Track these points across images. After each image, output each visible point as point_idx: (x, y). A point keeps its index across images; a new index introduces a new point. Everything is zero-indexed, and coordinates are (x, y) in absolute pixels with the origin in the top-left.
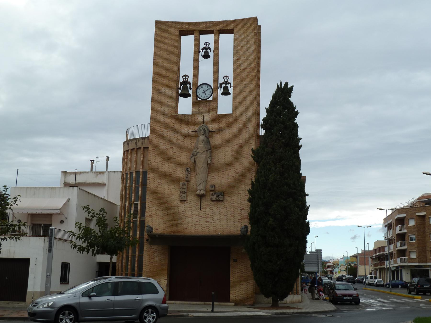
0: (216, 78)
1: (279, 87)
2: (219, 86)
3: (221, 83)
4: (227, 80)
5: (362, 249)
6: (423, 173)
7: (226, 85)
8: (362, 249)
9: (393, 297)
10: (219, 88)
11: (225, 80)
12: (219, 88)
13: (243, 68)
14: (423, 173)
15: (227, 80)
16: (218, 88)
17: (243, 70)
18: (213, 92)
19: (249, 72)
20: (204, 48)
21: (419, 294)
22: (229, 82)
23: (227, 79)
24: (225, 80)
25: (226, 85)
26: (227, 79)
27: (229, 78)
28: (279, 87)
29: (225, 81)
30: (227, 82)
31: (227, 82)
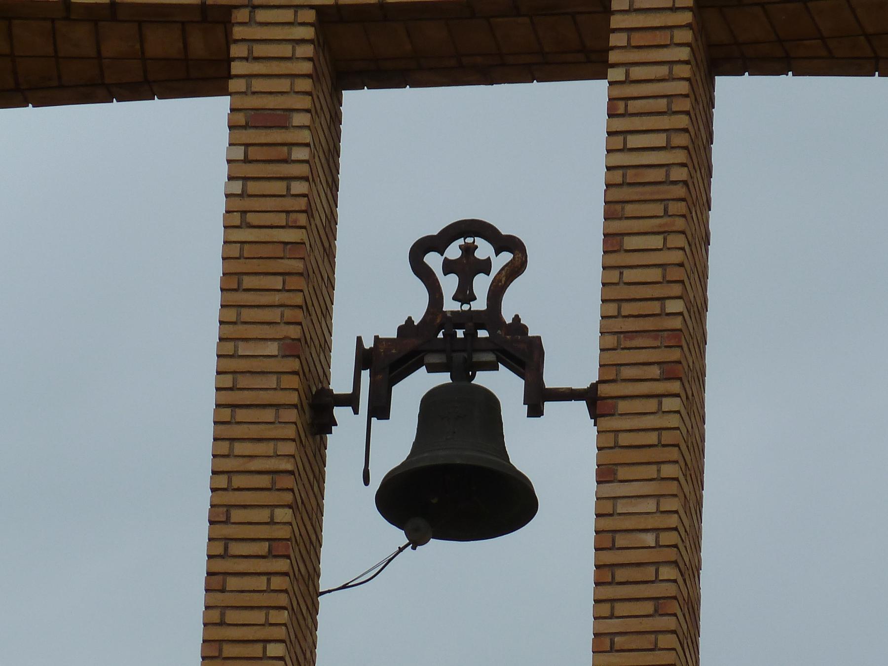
4: (480, 304)
5: (359, 340)
8: (359, 340)
12: (340, 413)
20: (407, 329)
23: (482, 284)
24: (450, 305)
26: (482, 284)
29: (459, 319)
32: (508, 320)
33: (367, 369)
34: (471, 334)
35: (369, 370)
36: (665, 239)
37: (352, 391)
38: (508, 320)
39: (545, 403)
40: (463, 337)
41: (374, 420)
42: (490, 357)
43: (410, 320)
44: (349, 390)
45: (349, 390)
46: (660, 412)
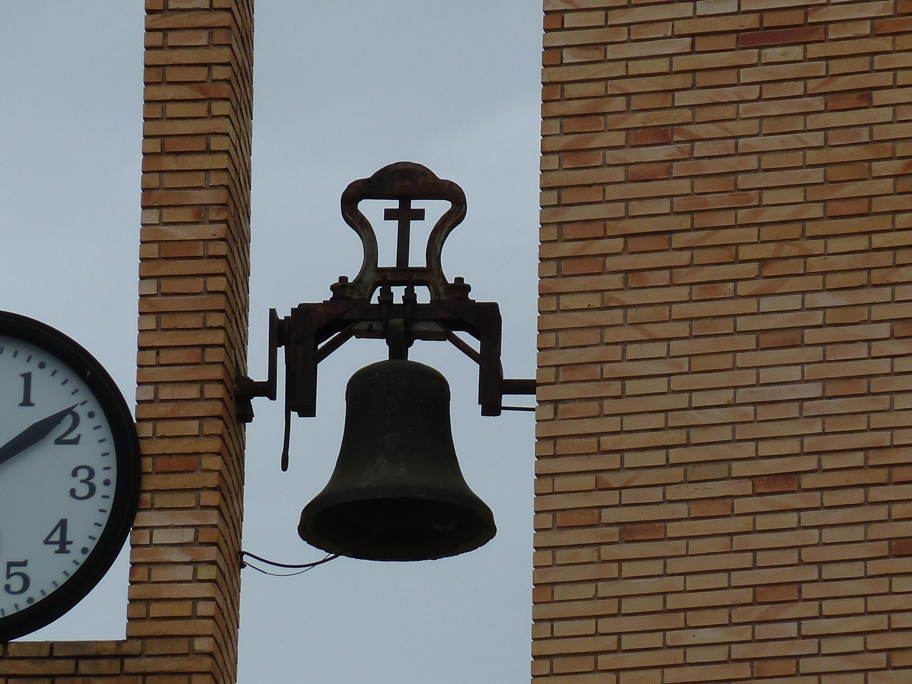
0: (200, 214)
1: (10, 641)
2: (257, 371)
3: (303, 312)
4: (417, 259)
5: (273, 313)
6: (285, 467)
7: (398, 350)
8: (273, 313)
9: (320, 347)
10: (258, 403)
11: (387, 259)
12: (258, 403)
13: (751, 21)
14: (285, 467)
15: (417, 259)
16: (247, 415)
17: (752, 55)
18: (149, 483)
19: (865, 96)
20: (341, 287)
21: (281, 351)
22: (461, 287)
23: (420, 232)
24: (387, 259)
25: (398, 350)
26: (420, 232)
27: (455, 217)
28: (10, 641)
29: (387, 278)
30: (423, 295)
31: (423, 295)
32: (451, 281)
33: (379, 301)
34: (410, 297)
35: (378, 303)
36: (805, 50)
37: (267, 379)
38: (451, 281)
39: (503, 396)
40: (403, 303)
41: (294, 415)
42: (435, 327)
43: (343, 279)
44: (264, 378)
45: (264, 378)
46: (671, 250)
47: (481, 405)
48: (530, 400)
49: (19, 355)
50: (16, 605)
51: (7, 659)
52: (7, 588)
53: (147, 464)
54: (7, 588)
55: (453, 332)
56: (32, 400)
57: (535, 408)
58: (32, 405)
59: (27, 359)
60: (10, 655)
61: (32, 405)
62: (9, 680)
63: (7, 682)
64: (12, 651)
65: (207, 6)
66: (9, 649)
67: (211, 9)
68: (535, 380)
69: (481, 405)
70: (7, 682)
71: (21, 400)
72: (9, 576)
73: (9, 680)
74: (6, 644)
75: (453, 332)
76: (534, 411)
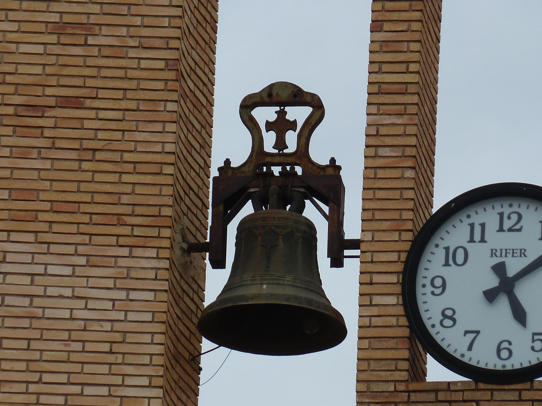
35: (305, 200)
47: (330, 258)
48: (357, 252)
49: (521, 206)
50: (495, 365)
51: (533, 390)
52: (533, 348)
53: (398, 289)
54: (533, 348)
55: (328, 215)
56: (486, 239)
57: (359, 256)
58: (486, 242)
59: (527, 207)
60: (535, 388)
61: (486, 242)
62: (534, 403)
63: (533, 404)
64: (536, 385)
65: (168, 4)
66: (534, 384)
67: (171, 6)
68: (360, 239)
69: (330, 258)
70: (533, 404)
71: (468, 239)
72: (533, 341)
73: (534, 403)
74: (532, 381)
75: (328, 215)
76: (359, 258)
